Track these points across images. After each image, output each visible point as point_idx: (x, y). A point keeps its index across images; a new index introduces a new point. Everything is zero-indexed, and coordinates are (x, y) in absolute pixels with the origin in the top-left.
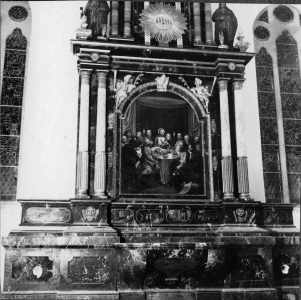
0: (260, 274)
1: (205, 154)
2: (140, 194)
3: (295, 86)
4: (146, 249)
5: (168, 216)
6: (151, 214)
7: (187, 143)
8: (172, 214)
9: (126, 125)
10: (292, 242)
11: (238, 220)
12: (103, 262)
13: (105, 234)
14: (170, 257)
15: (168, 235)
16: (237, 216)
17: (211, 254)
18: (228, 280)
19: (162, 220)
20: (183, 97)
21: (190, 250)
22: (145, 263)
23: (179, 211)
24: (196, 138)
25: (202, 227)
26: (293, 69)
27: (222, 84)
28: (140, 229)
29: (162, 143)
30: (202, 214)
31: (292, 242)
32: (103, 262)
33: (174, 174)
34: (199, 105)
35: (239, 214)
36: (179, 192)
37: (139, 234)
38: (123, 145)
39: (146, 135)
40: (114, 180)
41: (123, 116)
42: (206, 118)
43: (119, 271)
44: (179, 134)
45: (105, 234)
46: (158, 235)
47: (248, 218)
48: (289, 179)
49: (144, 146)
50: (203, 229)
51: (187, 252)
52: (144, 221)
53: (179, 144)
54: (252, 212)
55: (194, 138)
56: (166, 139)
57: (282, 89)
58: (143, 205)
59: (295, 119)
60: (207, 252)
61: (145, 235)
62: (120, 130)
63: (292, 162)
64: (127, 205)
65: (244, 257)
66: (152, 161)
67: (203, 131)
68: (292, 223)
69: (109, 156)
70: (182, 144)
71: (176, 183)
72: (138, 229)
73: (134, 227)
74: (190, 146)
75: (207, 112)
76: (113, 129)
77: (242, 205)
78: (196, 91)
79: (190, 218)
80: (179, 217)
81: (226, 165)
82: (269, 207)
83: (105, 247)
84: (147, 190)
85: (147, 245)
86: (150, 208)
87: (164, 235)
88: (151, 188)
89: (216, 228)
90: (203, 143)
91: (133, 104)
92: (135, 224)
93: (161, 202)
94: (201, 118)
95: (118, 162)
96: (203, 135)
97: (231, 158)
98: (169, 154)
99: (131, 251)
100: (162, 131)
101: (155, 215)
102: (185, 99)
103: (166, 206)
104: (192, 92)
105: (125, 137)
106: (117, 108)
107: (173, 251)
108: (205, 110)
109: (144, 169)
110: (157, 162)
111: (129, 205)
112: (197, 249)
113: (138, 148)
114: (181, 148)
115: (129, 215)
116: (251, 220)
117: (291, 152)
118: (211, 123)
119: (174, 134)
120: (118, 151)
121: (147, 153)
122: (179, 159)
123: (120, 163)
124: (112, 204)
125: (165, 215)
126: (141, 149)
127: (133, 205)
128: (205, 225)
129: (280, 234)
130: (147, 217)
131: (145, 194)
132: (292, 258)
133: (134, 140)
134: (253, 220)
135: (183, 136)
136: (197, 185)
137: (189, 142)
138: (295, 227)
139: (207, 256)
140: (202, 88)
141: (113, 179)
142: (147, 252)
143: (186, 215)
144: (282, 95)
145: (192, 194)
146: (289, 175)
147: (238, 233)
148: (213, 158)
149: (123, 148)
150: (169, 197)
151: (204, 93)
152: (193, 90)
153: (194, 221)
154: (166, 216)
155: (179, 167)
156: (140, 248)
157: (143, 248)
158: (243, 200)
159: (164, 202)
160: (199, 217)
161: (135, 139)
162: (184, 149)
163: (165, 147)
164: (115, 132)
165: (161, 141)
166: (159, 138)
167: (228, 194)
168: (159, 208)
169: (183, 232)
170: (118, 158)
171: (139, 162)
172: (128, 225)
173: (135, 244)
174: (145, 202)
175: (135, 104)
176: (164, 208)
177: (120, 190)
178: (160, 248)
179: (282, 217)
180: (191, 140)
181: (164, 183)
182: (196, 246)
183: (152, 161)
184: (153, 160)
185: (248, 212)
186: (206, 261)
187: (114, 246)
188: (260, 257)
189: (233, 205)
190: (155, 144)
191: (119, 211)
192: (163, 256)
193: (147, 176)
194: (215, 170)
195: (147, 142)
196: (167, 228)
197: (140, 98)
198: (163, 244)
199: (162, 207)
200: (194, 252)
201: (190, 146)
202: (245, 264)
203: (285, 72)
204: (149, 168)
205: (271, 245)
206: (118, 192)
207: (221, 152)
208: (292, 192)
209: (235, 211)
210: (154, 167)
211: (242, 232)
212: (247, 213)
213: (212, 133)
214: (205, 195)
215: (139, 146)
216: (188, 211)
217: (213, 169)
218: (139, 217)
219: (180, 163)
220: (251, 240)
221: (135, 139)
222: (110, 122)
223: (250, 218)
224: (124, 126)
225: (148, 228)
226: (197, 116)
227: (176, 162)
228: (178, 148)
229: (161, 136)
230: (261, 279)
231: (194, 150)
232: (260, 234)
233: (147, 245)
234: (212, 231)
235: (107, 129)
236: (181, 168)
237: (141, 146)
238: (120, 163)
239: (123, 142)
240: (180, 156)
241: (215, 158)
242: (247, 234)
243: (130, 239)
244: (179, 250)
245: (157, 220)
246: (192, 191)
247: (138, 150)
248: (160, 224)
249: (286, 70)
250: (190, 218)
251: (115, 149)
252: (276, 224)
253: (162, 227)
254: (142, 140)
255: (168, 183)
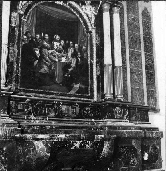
0: (133, 161)
1: (90, 61)
2: (38, 90)
3: (136, 29)
4: (51, 140)
5: (61, 110)
6: (47, 109)
7: (77, 50)
8: (64, 109)
9: (27, 26)
10: (151, 136)
11: (116, 117)
12: (2, 154)
13: (5, 125)
14: (72, 148)
15: (62, 127)
16: (116, 113)
17: (107, 145)
18: (111, 167)
19: (56, 114)
20: (75, 12)
21: (89, 141)
22: (49, 154)
23: (70, 107)
24: (84, 47)
25: (88, 121)
26: (136, 17)
27: (106, 6)
28: (37, 121)
29: (57, 47)
30: (87, 111)
31: (151, 136)
32: (2, 154)
33: (66, 76)
34: (87, 20)
35: (117, 111)
36: (70, 91)
37: (37, 126)
38: (23, 43)
39: (43, 38)
40: (14, 74)
41: (25, 18)
42: (92, 32)
43: (20, 163)
44: (71, 42)
45: (5, 125)
46: (54, 127)
47: (123, 116)
48: (132, 94)
49: (42, 48)
50: (89, 123)
51: (87, 143)
52: (41, 115)
53: (71, 51)
54: (126, 110)
55: (82, 48)
56: (60, 45)
57: (129, 29)
58: (40, 100)
59: (136, 50)
60: (104, 143)
61: (42, 127)
62: (22, 29)
63: (133, 80)
64: (26, 99)
65: (122, 147)
66: (48, 62)
67: (89, 42)
68: (148, 121)
69: (10, 51)
70: (73, 50)
71: (68, 84)
72: (36, 121)
73: (31, 119)
74: (79, 54)
75: (93, 27)
76: (15, 27)
77: (120, 105)
78: (86, 9)
79: (78, 114)
80: (70, 112)
81: (107, 70)
82: (134, 108)
83: (5, 138)
84: (44, 87)
85: (53, 136)
86: (46, 103)
87: (59, 127)
88: (48, 85)
89: (98, 123)
90: (89, 52)
91: (33, 9)
92: (33, 117)
93: (56, 98)
94: (88, 32)
95: (18, 58)
96: (89, 46)
97: (111, 66)
98: (62, 58)
99: (36, 143)
100: (58, 38)
101: (51, 110)
102: (76, 14)
103: (60, 102)
104: (82, 9)
105: (25, 37)
106: (20, 8)
107: (75, 142)
108: (92, 25)
109: (41, 68)
110: (52, 63)
111: (28, 98)
112: (95, 140)
113: (37, 49)
114: (72, 54)
115: (28, 108)
116: (125, 117)
117: (133, 72)
118: (96, 37)
119: (67, 42)
120: (19, 49)
121: (44, 54)
122: (71, 63)
123: (20, 60)
124: (12, 97)
125: (59, 110)
126: (39, 50)
127: (32, 99)
128: (90, 120)
129: (143, 129)
130: (43, 111)
131: (42, 91)
132: (150, 148)
133: (34, 41)
134: (127, 117)
135: (74, 44)
136: (84, 86)
137: (78, 50)
138: (150, 124)
139: (103, 147)
140: (91, 7)
141: (13, 73)
142: (52, 143)
143: (76, 111)
144: (129, 33)
145: (80, 93)
146: (132, 88)
147: (119, 127)
148: (97, 65)
149: (23, 46)
150: (62, 95)
151: (91, 12)
152: (83, 7)
153: (82, 116)
154: (60, 111)
155: (70, 70)
156: (46, 139)
157: (49, 140)
158: (120, 100)
159: (59, 99)
160: (86, 113)
161: (35, 40)
162: (74, 55)
163: (59, 51)
164: (17, 29)
165: (57, 45)
166: (55, 43)
167: (108, 95)
168: (54, 104)
169: (74, 125)
170: (18, 54)
171: (37, 61)
172: (26, 117)
173: (40, 136)
174: (43, 97)
175: (35, 9)
176: (58, 104)
177: (19, 85)
178: (65, 139)
179: (142, 116)
180: (80, 48)
181: (58, 82)
182: (96, 138)
183: (48, 62)
184: (49, 61)
185: (124, 110)
186: (102, 150)
187: (15, 138)
188: (133, 147)
189: (113, 104)
190: (52, 47)
191: (18, 103)
192: (66, 147)
193: (44, 75)
194: (98, 75)
195: (45, 45)
196: (61, 121)
197: (40, 5)
198: (68, 135)
199: (57, 102)
200: (93, 144)
201: (79, 54)
202: (123, 153)
203: (131, 17)
204: (46, 68)
205: (141, 137)
206: (17, 86)
207: (104, 61)
208: (134, 100)
209: (115, 109)
210: (50, 67)
211: (121, 126)
212: (122, 111)
213: (96, 45)
214: (90, 95)
215: (37, 47)
216: (77, 107)
217: (97, 74)
218: (36, 110)
219: (71, 66)
220: (128, 133)
221: (35, 40)
222: (13, 19)
223: (125, 115)
224: (25, 26)
225: (44, 121)
226: (85, 30)
227: (67, 65)
228: (70, 54)
229: (56, 41)
230: (134, 165)
231: (82, 57)
232: (133, 128)
233: (53, 136)
234: (96, 125)
235: (10, 26)
236: (72, 70)
237: (39, 47)
238: (20, 60)
239: (23, 41)
240: (71, 61)
241: (98, 65)
242: (125, 128)
243: (29, 131)
244: (81, 142)
245: (52, 115)
246: (80, 91)
247: (37, 50)
248: (55, 117)
249: (131, 16)
250: (78, 114)
251: (16, 45)
252: (138, 121)
253: (56, 120)
254: (41, 42)
255: (61, 83)
